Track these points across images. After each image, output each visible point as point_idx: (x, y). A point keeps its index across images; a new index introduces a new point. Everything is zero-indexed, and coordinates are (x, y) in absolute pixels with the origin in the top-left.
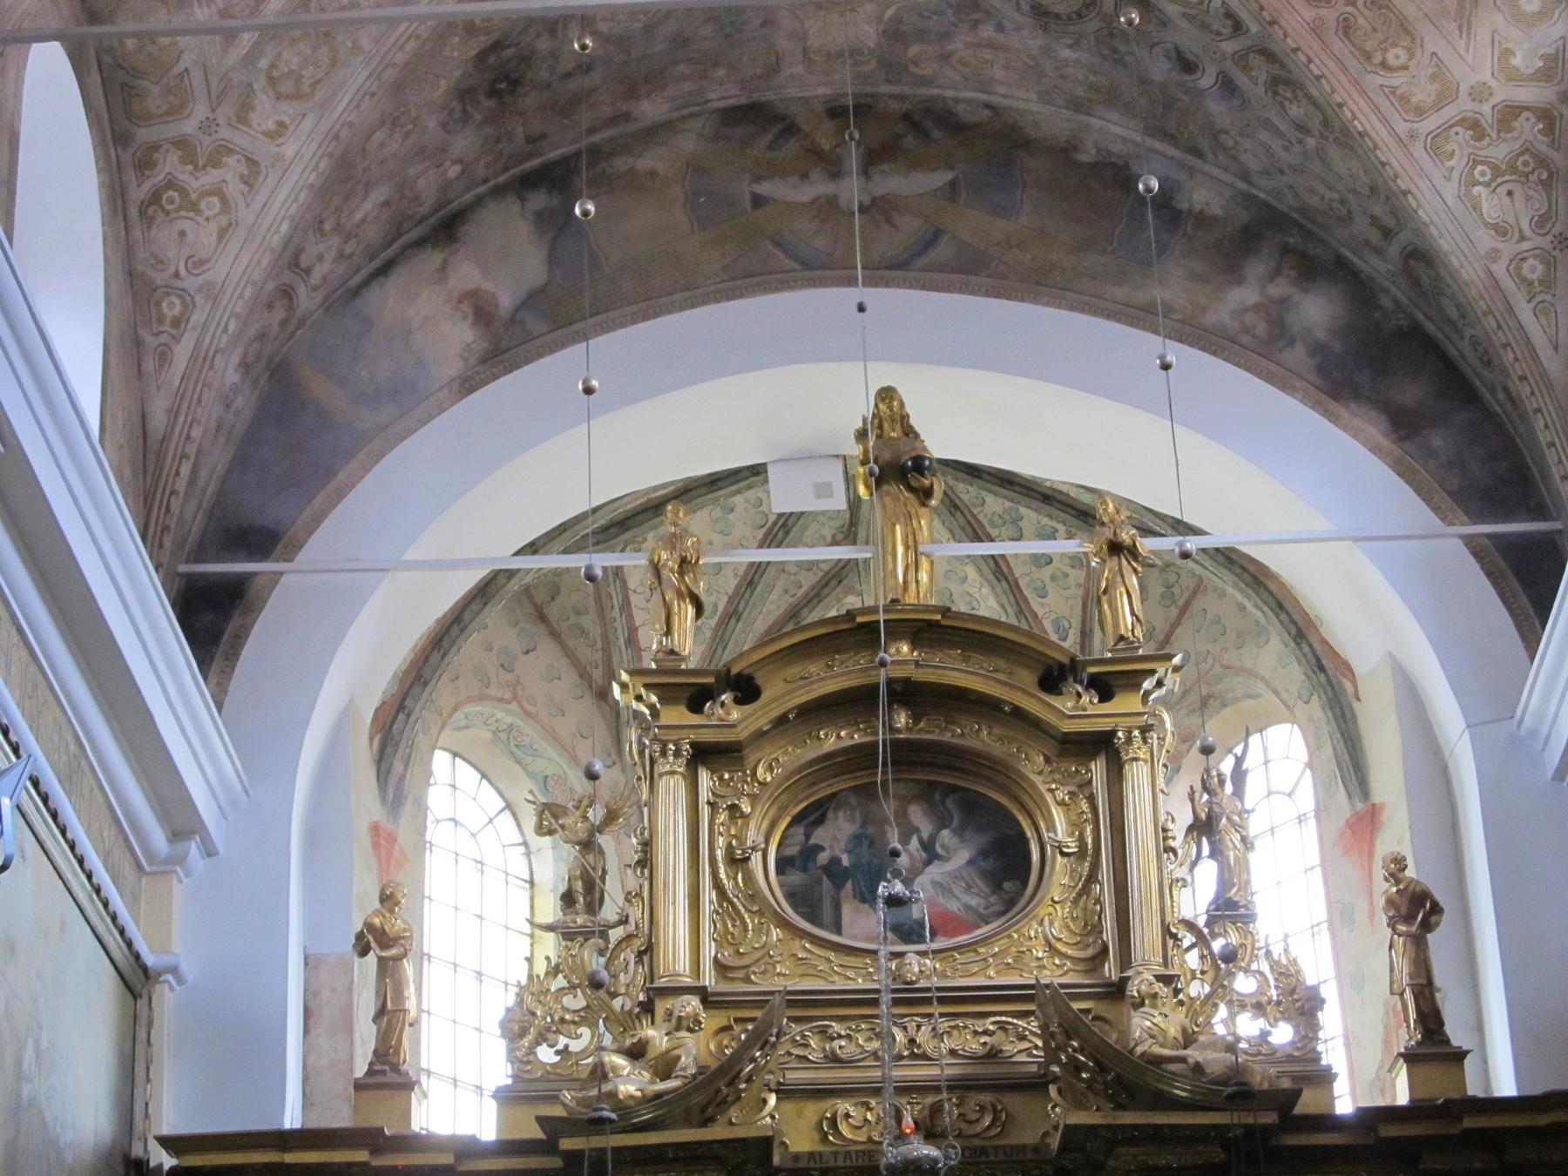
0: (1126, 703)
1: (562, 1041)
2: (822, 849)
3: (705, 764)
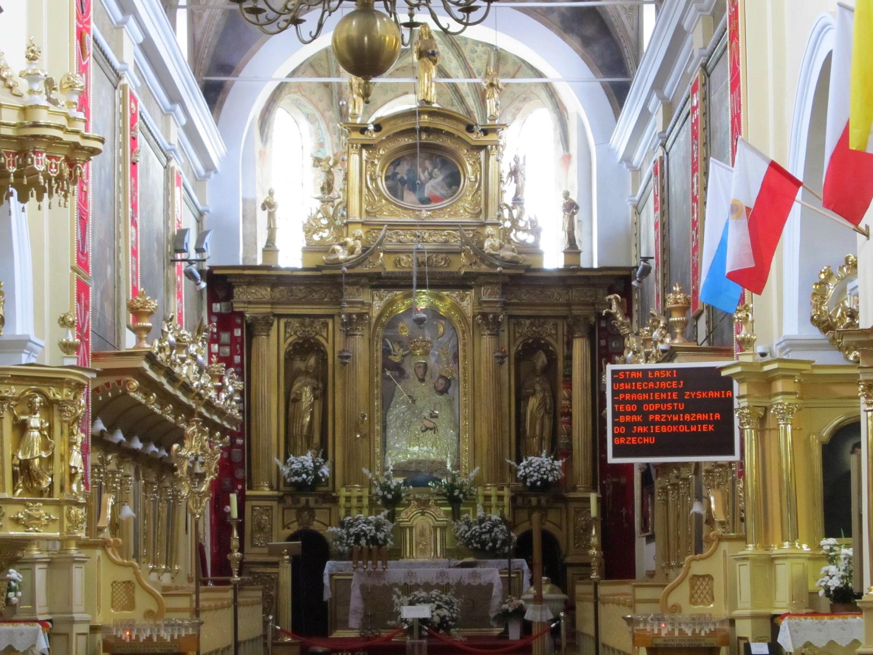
0: (491, 137)
1: (321, 234)
3: (365, 148)
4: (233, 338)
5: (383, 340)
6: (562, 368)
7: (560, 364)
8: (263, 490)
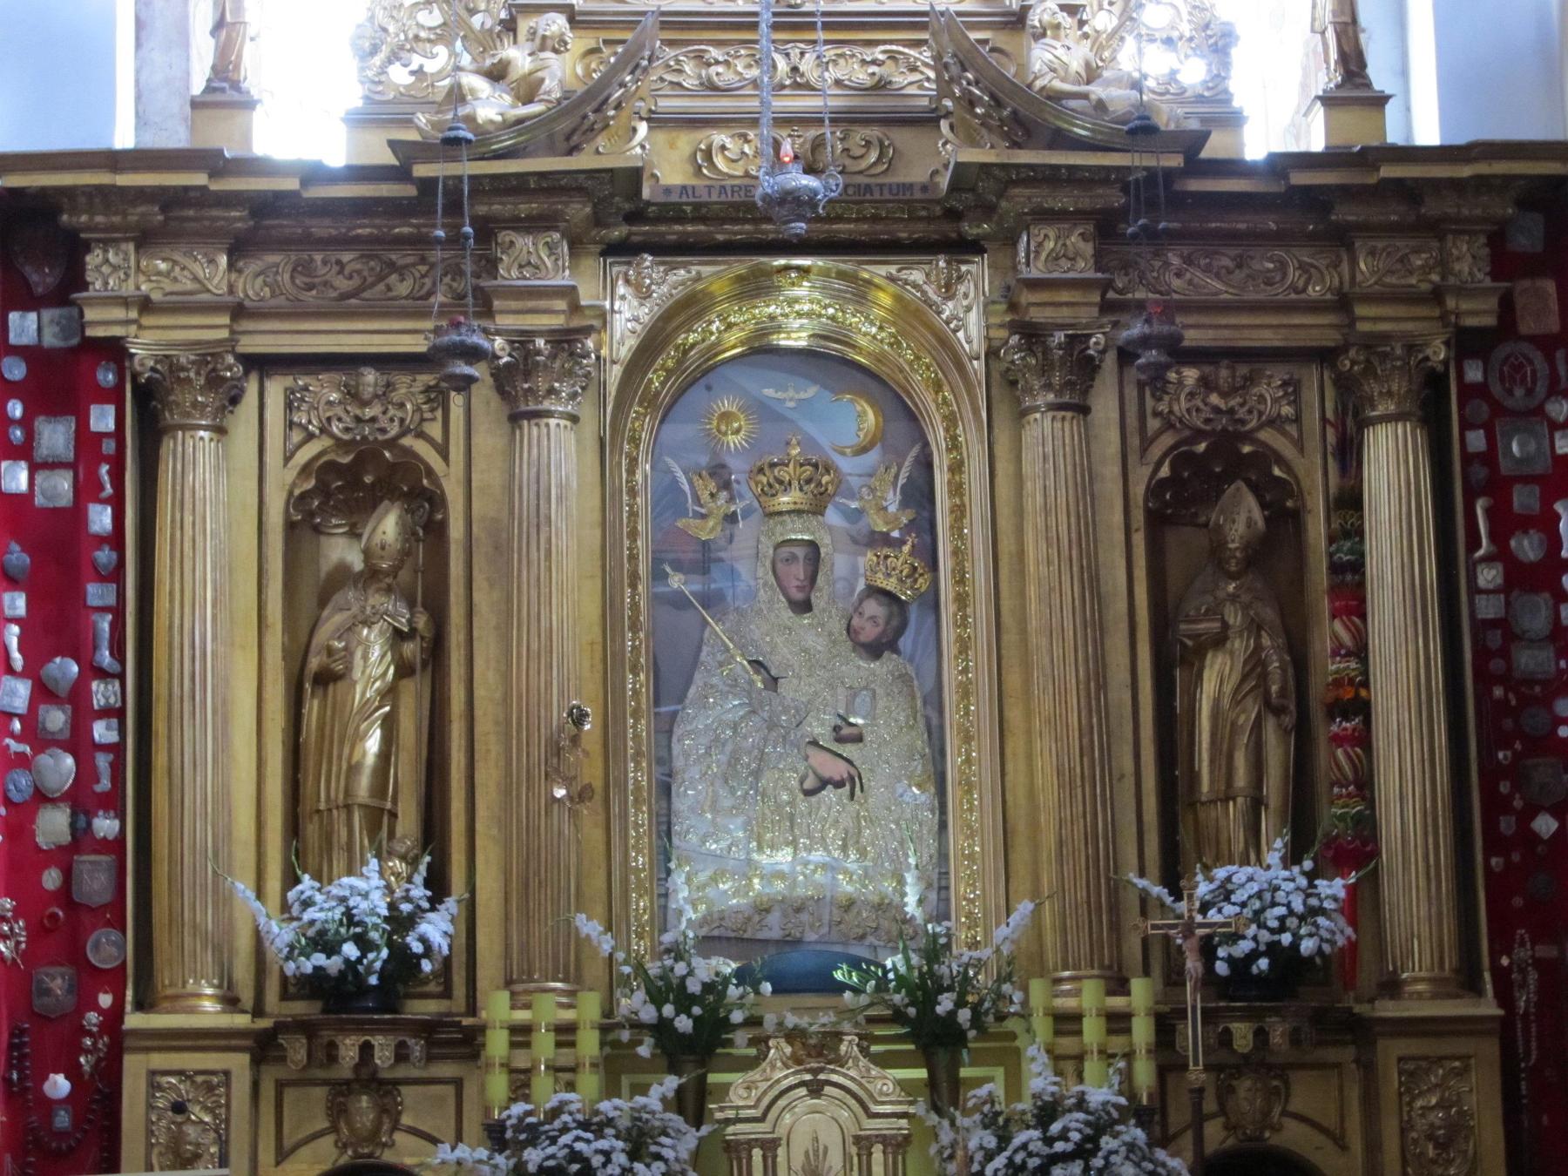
1: (416, 61)
4: (86, 441)
6: (1323, 543)
7: (1317, 528)
8: (193, 1011)
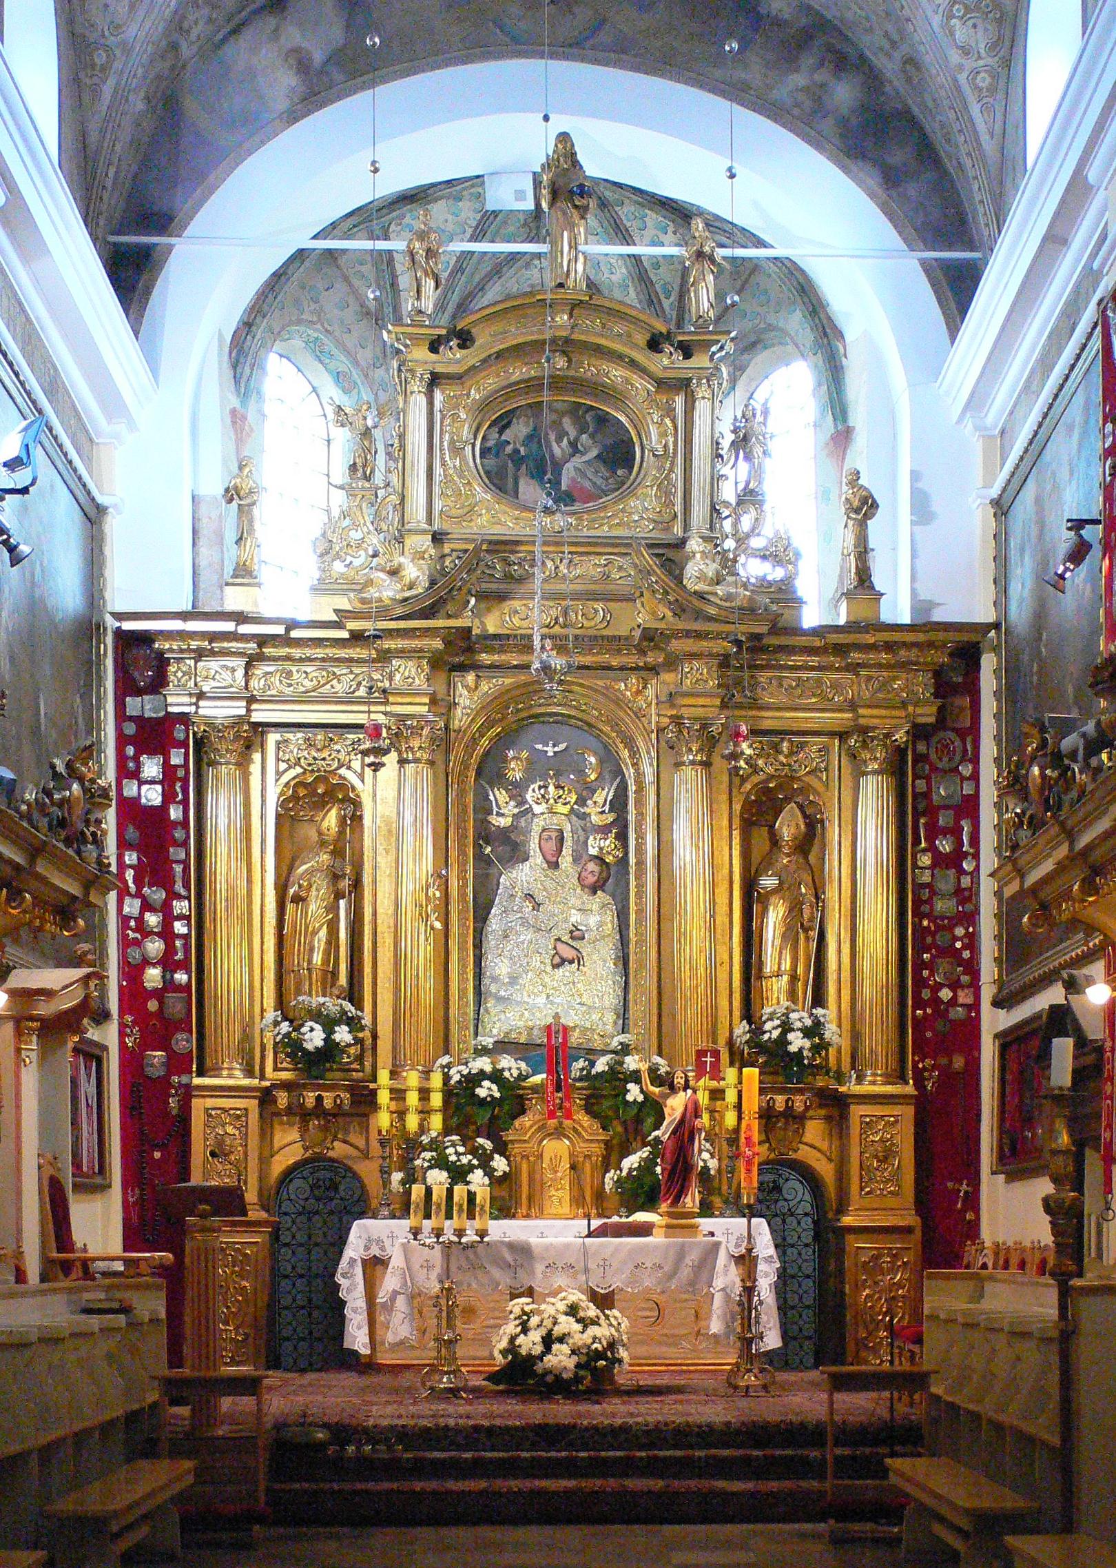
0: (700, 360)
2: (509, 443)
4: (168, 770)
5: (476, 688)
